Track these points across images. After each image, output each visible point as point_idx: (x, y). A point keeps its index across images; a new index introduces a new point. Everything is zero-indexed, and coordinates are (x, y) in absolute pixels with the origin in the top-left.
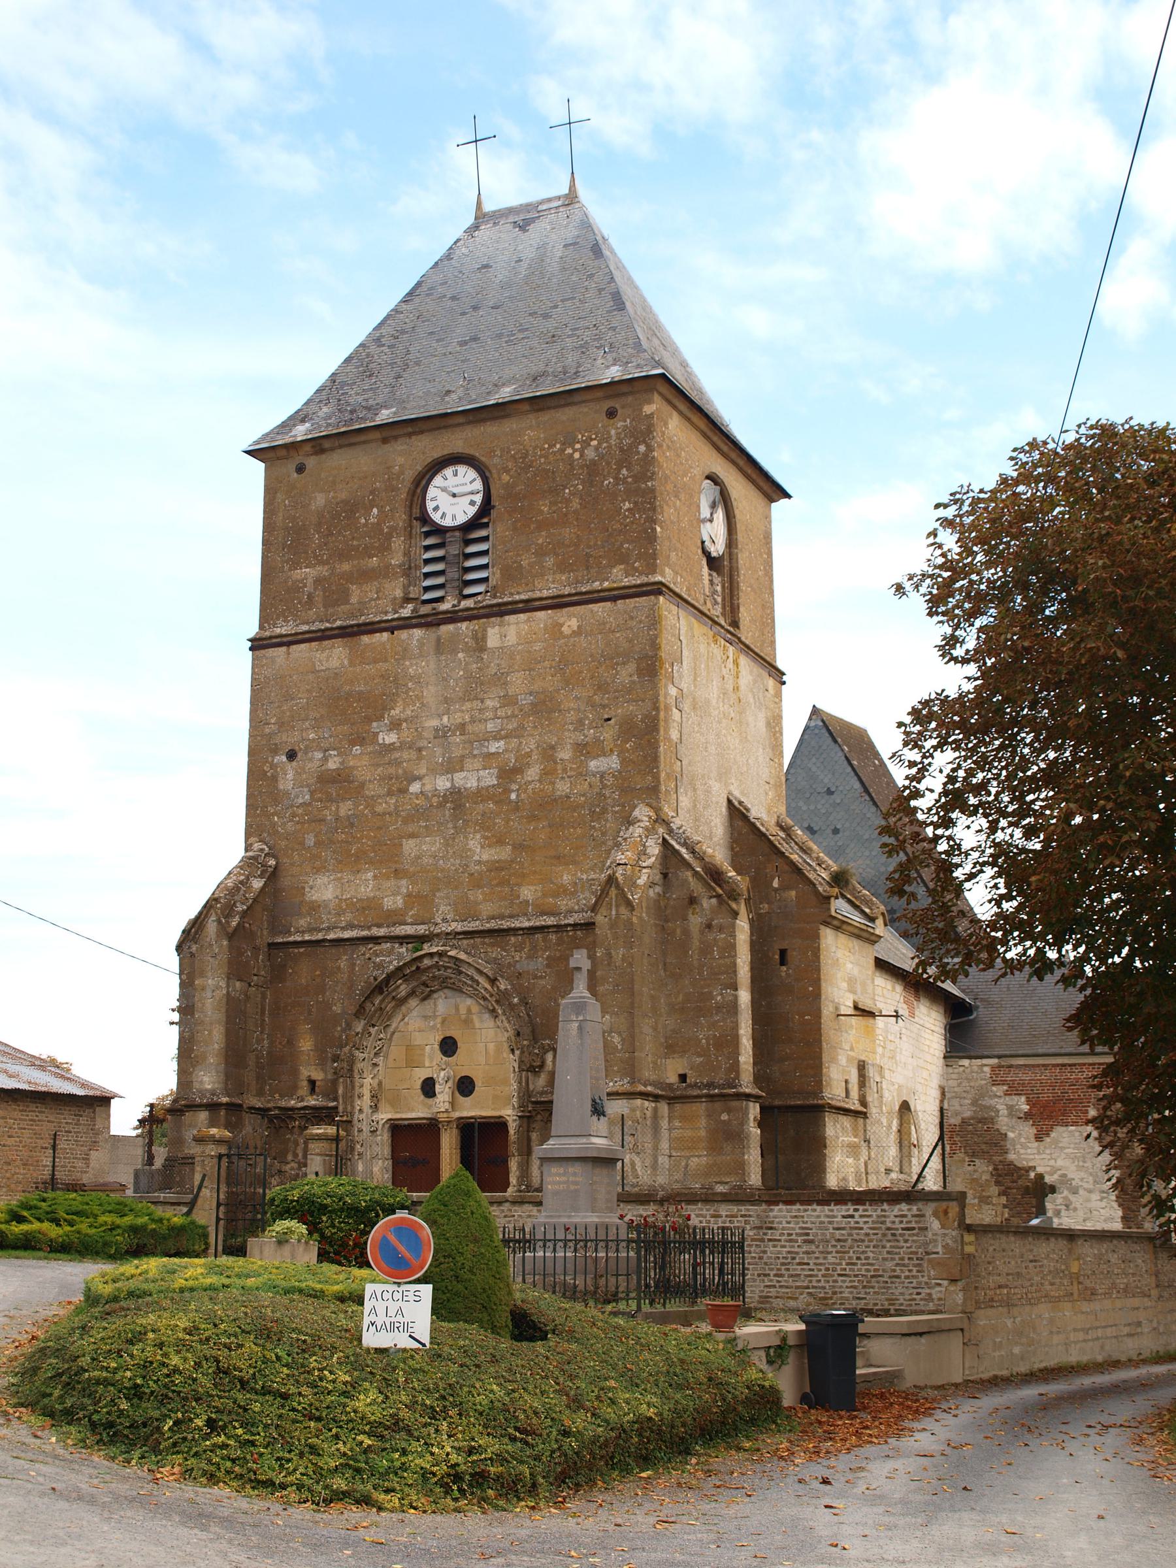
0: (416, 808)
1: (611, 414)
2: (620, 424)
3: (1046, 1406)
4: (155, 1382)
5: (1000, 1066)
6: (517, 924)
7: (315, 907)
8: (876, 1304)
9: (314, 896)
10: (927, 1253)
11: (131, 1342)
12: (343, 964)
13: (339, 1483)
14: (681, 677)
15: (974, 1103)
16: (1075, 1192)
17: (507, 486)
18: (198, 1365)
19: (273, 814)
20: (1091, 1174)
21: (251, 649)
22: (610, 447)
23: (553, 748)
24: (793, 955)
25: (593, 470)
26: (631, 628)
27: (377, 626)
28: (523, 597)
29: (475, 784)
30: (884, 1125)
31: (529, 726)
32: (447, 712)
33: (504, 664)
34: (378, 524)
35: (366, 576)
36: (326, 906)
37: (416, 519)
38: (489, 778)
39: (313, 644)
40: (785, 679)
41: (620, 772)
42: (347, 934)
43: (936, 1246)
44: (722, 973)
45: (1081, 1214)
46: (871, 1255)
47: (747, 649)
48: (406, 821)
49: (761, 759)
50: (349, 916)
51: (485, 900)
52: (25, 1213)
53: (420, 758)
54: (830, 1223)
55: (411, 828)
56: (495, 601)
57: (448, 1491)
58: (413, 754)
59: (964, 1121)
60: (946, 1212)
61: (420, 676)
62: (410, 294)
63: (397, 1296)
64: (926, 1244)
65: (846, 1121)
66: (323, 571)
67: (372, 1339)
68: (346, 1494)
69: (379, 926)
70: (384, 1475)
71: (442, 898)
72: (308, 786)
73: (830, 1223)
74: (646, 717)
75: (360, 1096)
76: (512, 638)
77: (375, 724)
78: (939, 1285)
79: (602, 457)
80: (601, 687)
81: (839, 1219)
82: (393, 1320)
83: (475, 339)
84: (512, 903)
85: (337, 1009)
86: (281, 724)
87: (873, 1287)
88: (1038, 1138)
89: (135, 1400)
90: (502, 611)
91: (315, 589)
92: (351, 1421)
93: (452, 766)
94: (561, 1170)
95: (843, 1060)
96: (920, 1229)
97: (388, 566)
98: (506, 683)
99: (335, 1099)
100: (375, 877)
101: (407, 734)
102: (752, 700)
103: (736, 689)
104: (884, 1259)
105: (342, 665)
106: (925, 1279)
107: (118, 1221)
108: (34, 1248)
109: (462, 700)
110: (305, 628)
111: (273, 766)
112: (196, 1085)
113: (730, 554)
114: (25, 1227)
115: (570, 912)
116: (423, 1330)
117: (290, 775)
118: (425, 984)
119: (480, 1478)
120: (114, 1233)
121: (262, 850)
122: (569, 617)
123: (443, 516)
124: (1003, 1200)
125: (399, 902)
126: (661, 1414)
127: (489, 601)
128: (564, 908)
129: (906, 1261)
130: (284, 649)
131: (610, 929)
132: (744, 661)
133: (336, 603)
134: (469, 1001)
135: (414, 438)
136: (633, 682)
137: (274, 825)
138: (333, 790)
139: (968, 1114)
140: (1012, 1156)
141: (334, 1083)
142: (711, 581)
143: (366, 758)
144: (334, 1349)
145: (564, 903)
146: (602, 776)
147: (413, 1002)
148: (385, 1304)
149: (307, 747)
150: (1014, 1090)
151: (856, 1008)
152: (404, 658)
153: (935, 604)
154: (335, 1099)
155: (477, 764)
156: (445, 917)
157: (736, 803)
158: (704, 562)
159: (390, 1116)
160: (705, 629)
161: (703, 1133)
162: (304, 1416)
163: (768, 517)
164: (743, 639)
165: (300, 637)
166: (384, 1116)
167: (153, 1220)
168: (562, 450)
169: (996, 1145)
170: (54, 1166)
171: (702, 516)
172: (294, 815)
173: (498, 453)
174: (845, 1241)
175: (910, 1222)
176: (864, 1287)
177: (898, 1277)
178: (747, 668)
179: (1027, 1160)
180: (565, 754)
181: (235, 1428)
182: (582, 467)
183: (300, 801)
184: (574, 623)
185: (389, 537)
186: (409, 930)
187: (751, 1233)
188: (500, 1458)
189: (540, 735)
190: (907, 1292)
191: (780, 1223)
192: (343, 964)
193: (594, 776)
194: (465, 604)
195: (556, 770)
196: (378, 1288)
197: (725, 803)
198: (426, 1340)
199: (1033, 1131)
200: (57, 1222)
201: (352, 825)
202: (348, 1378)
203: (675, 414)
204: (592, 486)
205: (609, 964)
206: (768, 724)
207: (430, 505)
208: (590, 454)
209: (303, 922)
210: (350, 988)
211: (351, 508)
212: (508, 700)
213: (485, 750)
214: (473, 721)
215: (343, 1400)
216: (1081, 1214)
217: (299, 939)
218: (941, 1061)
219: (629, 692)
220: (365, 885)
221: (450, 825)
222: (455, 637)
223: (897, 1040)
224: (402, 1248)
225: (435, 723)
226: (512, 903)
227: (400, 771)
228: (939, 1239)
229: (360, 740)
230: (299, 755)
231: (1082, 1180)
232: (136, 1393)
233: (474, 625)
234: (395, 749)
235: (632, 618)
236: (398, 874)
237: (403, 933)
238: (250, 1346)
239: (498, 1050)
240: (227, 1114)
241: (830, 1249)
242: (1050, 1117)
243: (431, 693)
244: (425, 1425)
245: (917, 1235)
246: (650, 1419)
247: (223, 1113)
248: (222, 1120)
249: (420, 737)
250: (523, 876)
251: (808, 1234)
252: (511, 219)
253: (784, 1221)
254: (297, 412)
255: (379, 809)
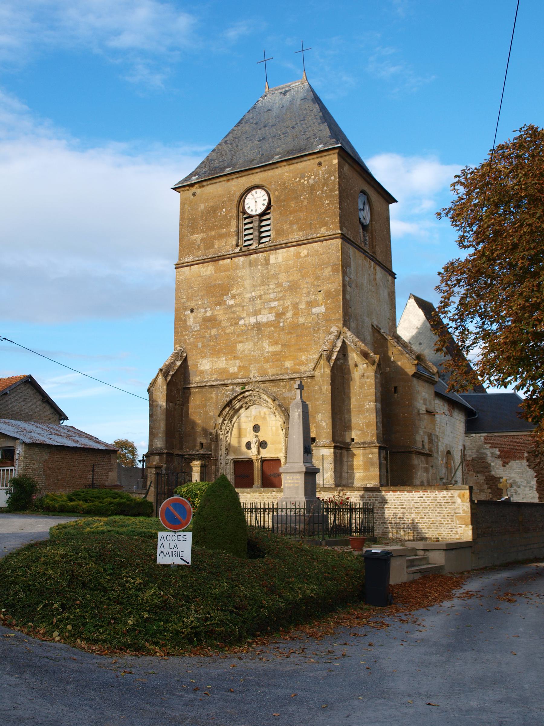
0: (242, 330)
1: (320, 164)
2: (323, 169)
3: (511, 583)
4: (39, 583)
5: (488, 436)
6: (283, 377)
7: (202, 373)
8: (433, 536)
9: (201, 368)
10: (455, 513)
11: (33, 562)
12: (213, 395)
13: (128, 640)
14: (351, 273)
15: (477, 451)
16: (519, 487)
17: (277, 197)
18: (62, 574)
19: (185, 335)
20: (525, 480)
21: (175, 268)
22: (319, 178)
23: (297, 304)
24: (400, 389)
25: (312, 188)
26: (329, 253)
27: (225, 257)
28: (284, 242)
29: (266, 320)
30: (440, 461)
31: (287, 295)
32: (254, 290)
33: (277, 270)
34: (225, 215)
35: (221, 236)
36: (206, 372)
37: (241, 212)
38: (272, 317)
39: (200, 265)
40: (396, 276)
41: (325, 313)
42: (215, 383)
43: (459, 510)
44: (369, 396)
45: (521, 496)
46: (430, 514)
47: (379, 263)
48: (238, 336)
49: (386, 309)
50: (215, 376)
51: (270, 368)
52: (74, 498)
53: (243, 310)
54: (413, 500)
55: (240, 339)
56: (273, 244)
57: (191, 642)
58: (241, 308)
59: (473, 459)
60: (463, 495)
61: (243, 276)
62: (239, 123)
63: (174, 538)
64: (455, 509)
65: (423, 458)
66: (204, 235)
67: (161, 560)
68: (129, 646)
69: (228, 379)
70: (153, 635)
71: (253, 367)
72: (199, 323)
73: (413, 500)
74: (335, 289)
75: (221, 449)
76: (280, 259)
77: (225, 297)
78: (461, 527)
79: (316, 182)
80: (317, 278)
81: (417, 498)
82: (172, 550)
83: (264, 139)
84: (281, 369)
85: (211, 414)
86: (188, 299)
87: (431, 528)
88: (504, 465)
89: (28, 593)
90: (276, 248)
91: (201, 243)
92: (140, 604)
93: (257, 313)
94: (291, 478)
95: (421, 432)
96: (452, 502)
97: (230, 232)
98: (278, 278)
99: (211, 451)
100: (226, 359)
101: (238, 300)
102: (382, 285)
103: (375, 279)
104: (436, 516)
105: (212, 273)
106: (455, 524)
107: (112, 500)
108: (76, 512)
109: (260, 285)
110: (197, 259)
111: (185, 316)
112: (154, 445)
113: (372, 224)
114: (73, 503)
115: (305, 372)
116: (188, 556)
117: (192, 319)
118: (246, 403)
119: (210, 634)
120: (111, 505)
121: (181, 350)
122: (304, 249)
123: (252, 210)
124: (490, 490)
125: (236, 369)
126: (318, 594)
127: (270, 244)
128: (303, 370)
129: (446, 517)
130: (189, 267)
131: (321, 377)
132: (378, 268)
133: (209, 248)
134: (265, 410)
135: (239, 179)
136: (330, 275)
137: (185, 340)
138: (209, 324)
139: (475, 456)
140: (493, 473)
141: (210, 444)
142: (364, 235)
143: (222, 311)
144: (138, 565)
145: (303, 368)
146: (318, 315)
147: (242, 411)
148: (168, 542)
149: (198, 307)
150: (493, 446)
151: (427, 411)
152: (236, 269)
153: (454, 219)
154: (211, 451)
155: (266, 311)
156: (254, 374)
157: (375, 327)
158: (361, 227)
159: (233, 457)
160: (361, 254)
161: (361, 463)
162: (114, 602)
163: (388, 210)
164: (378, 259)
165: (195, 262)
166: (231, 457)
167: (128, 500)
168: (300, 181)
169: (486, 468)
170: (93, 478)
171: (359, 208)
172: (193, 335)
173: (273, 183)
174: (419, 508)
175: (447, 500)
176: (428, 528)
177: (442, 524)
178: (380, 273)
179: (499, 474)
180: (302, 306)
181: (76, 609)
182: (308, 187)
183: (196, 329)
184: (305, 252)
185: (230, 220)
186: (240, 381)
187: (378, 505)
188: (222, 623)
189: (292, 299)
190: (446, 530)
191: (391, 500)
192: (213, 395)
193: (315, 315)
194: (261, 246)
195: (299, 313)
196: (165, 534)
197: (371, 326)
198: (189, 560)
199: (501, 463)
200: (86, 501)
201: (216, 338)
202: (141, 581)
203: (347, 165)
204: (312, 195)
205: (321, 393)
206: (389, 295)
207: (246, 207)
208: (311, 181)
209: (197, 379)
210: (216, 405)
211: (214, 209)
212: (279, 285)
213: (270, 306)
214: (265, 294)
215: (137, 593)
216: (521, 496)
217: (196, 386)
218: (464, 435)
219: (329, 280)
220: (222, 363)
221: (256, 337)
222: (257, 260)
223: (445, 426)
224: (176, 514)
225: (249, 295)
226: (281, 369)
227: (235, 316)
228: (461, 507)
229: (219, 304)
230: (195, 311)
231: (522, 482)
232: (28, 589)
233: (265, 254)
234: (233, 307)
235: (329, 249)
236: (235, 358)
237: (237, 382)
238: (92, 565)
239: (277, 430)
240: (166, 457)
241: (413, 512)
242: (508, 457)
243: (248, 283)
244: (182, 606)
245: (451, 505)
246: (312, 597)
247: (165, 456)
248: (165, 460)
249: (243, 301)
250: (286, 357)
251: (403, 505)
252: (280, 91)
253: (392, 499)
254: (193, 172)
255: (227, 331)
